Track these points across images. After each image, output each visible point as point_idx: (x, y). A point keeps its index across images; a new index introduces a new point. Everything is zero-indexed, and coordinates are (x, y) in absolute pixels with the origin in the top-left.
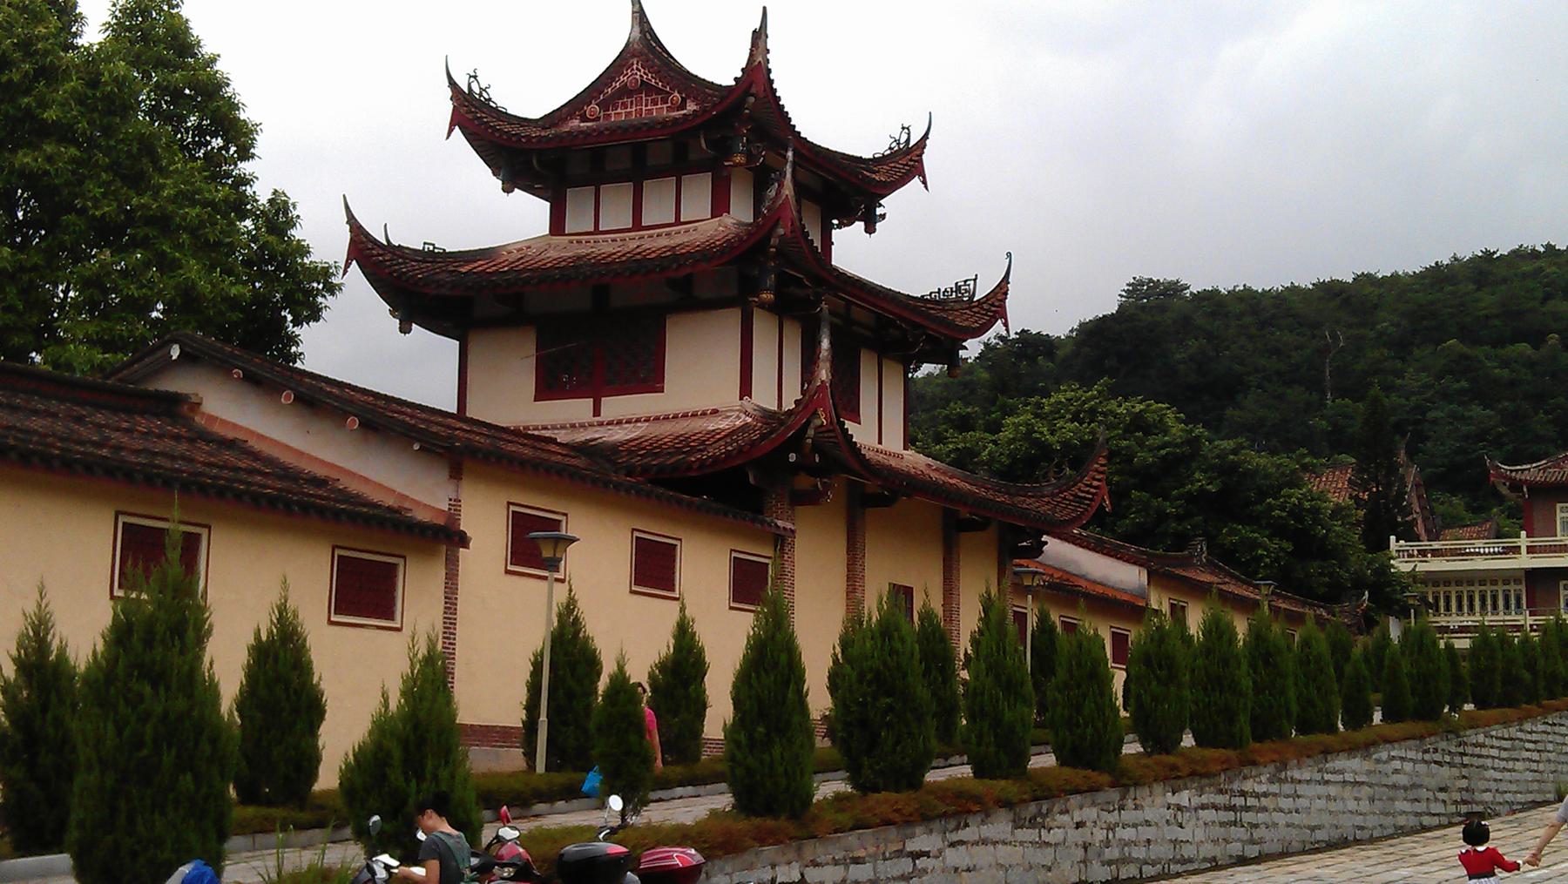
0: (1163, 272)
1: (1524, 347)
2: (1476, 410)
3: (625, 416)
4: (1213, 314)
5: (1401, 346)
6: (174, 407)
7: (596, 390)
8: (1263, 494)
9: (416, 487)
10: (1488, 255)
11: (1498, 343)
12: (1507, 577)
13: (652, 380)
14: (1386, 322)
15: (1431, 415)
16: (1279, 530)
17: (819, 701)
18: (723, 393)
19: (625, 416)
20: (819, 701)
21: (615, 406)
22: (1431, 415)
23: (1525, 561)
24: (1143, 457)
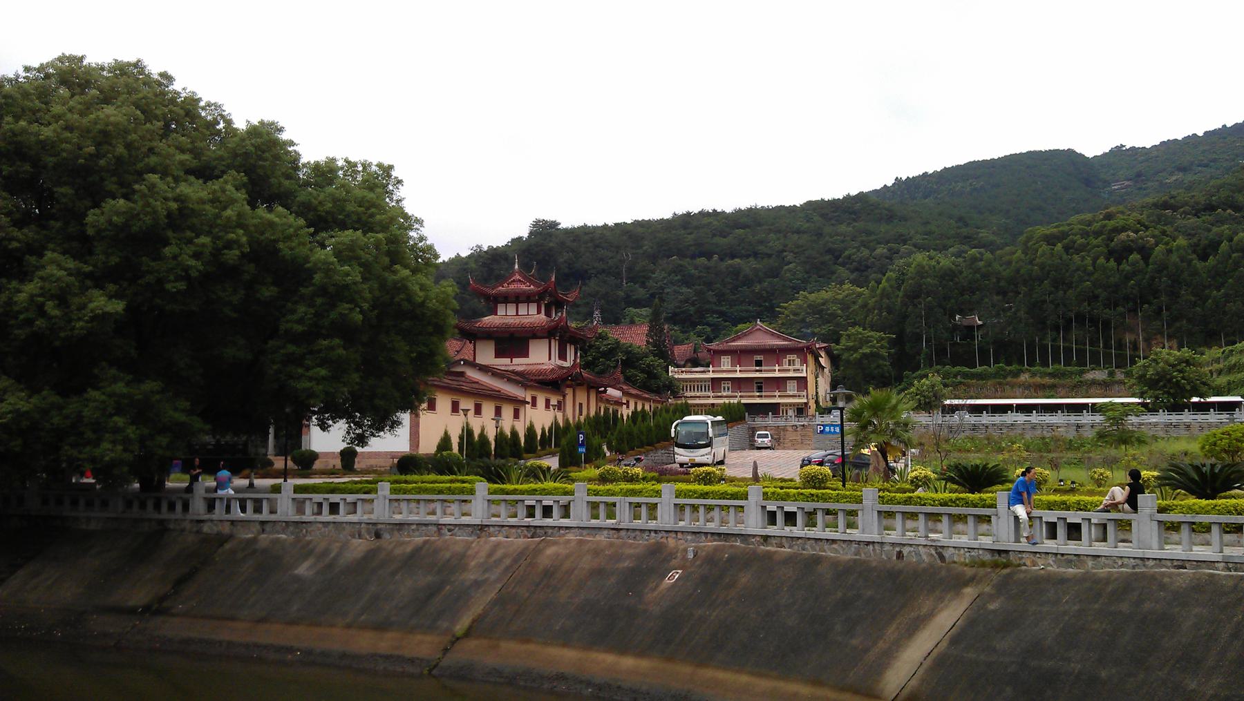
0: (549, 217)
1: (703, 260)
2: (684, 290)
3: (519, 364)
4: (574, 241)
5: (654, 258)
6: (462, 374)
7: (512, 357)
8: (638, 359)
9: (518, 392)
10: (689, 214)
11: (693, 257)
12: (705, 380)
13: (526, 355)
14: (647, 246)
15: (667, 290)
16: (643, 371)
17: (271, 430)
18: (545, 359)
19: (519, 364)
20: (271, 430)
21: (516, 361)
22: (667, 290)
23: (711, 375)
24: (603, 348)
